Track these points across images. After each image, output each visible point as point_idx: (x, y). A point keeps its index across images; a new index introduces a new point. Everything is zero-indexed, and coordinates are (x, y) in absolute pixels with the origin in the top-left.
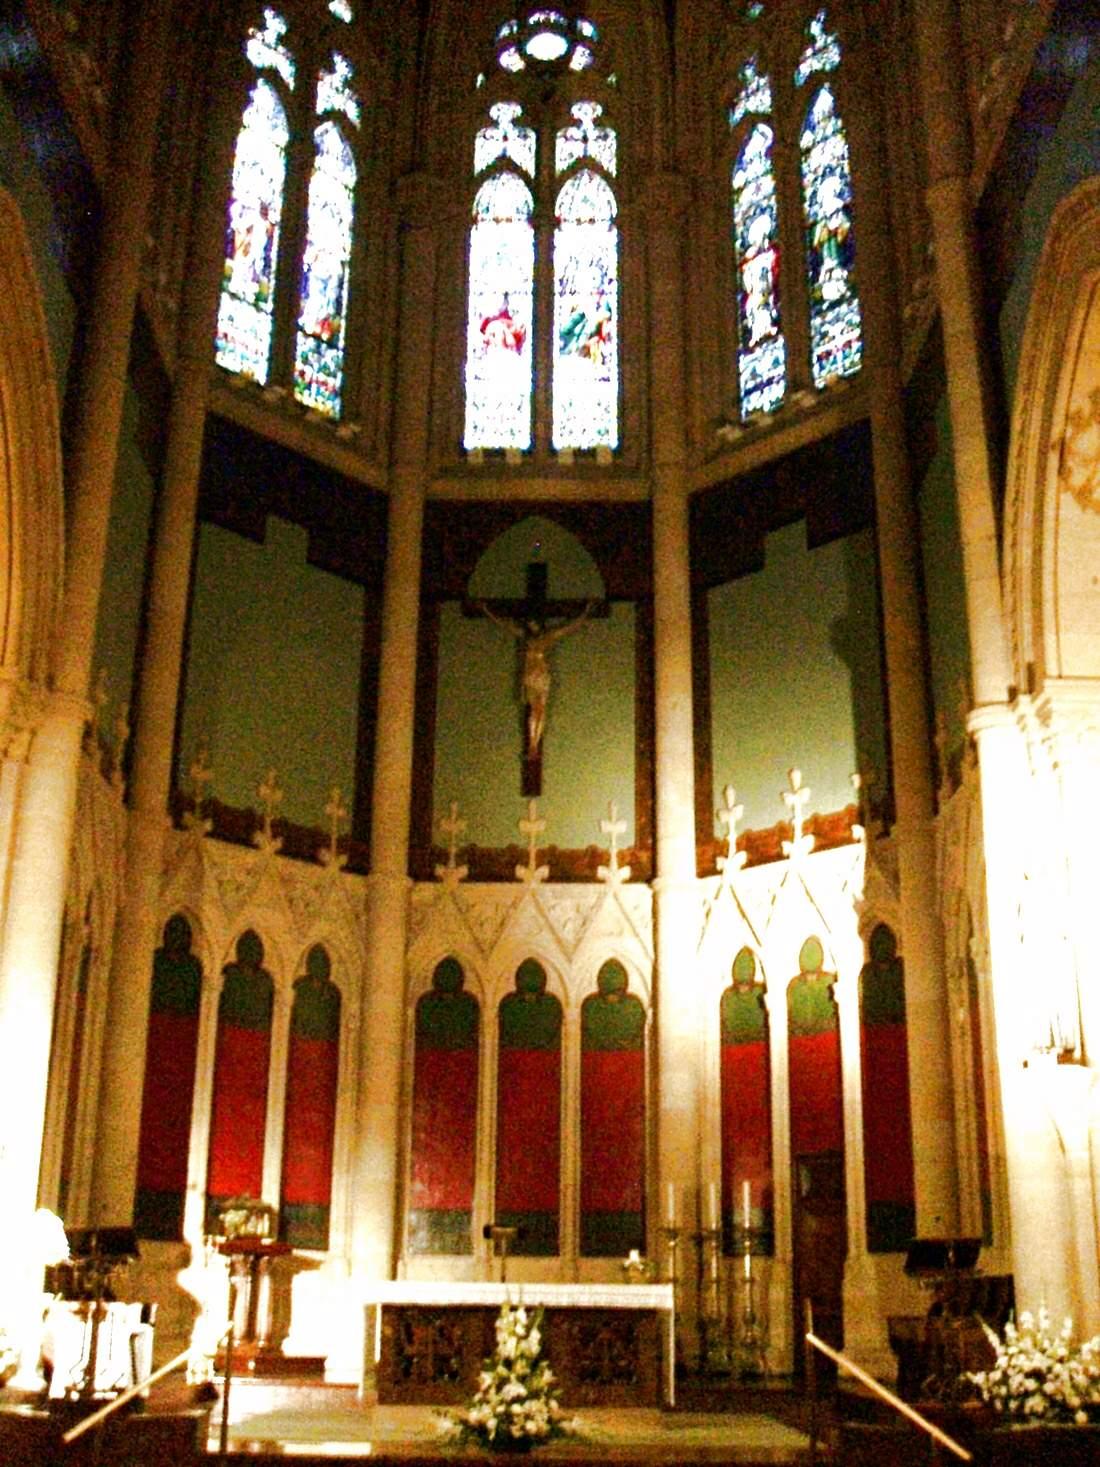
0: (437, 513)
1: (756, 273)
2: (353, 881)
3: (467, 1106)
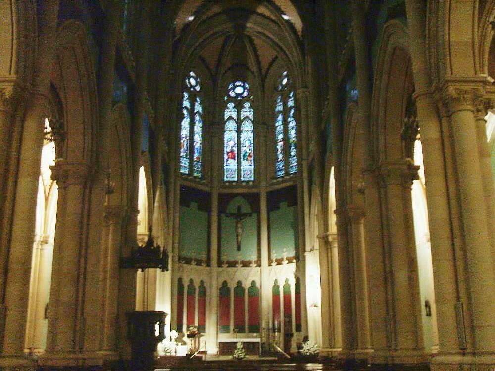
0: (221, 196)
1: (280, 145)
2: (208, 268)
3: (228, 313)
